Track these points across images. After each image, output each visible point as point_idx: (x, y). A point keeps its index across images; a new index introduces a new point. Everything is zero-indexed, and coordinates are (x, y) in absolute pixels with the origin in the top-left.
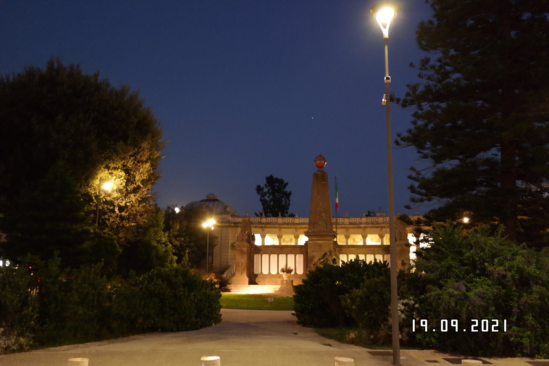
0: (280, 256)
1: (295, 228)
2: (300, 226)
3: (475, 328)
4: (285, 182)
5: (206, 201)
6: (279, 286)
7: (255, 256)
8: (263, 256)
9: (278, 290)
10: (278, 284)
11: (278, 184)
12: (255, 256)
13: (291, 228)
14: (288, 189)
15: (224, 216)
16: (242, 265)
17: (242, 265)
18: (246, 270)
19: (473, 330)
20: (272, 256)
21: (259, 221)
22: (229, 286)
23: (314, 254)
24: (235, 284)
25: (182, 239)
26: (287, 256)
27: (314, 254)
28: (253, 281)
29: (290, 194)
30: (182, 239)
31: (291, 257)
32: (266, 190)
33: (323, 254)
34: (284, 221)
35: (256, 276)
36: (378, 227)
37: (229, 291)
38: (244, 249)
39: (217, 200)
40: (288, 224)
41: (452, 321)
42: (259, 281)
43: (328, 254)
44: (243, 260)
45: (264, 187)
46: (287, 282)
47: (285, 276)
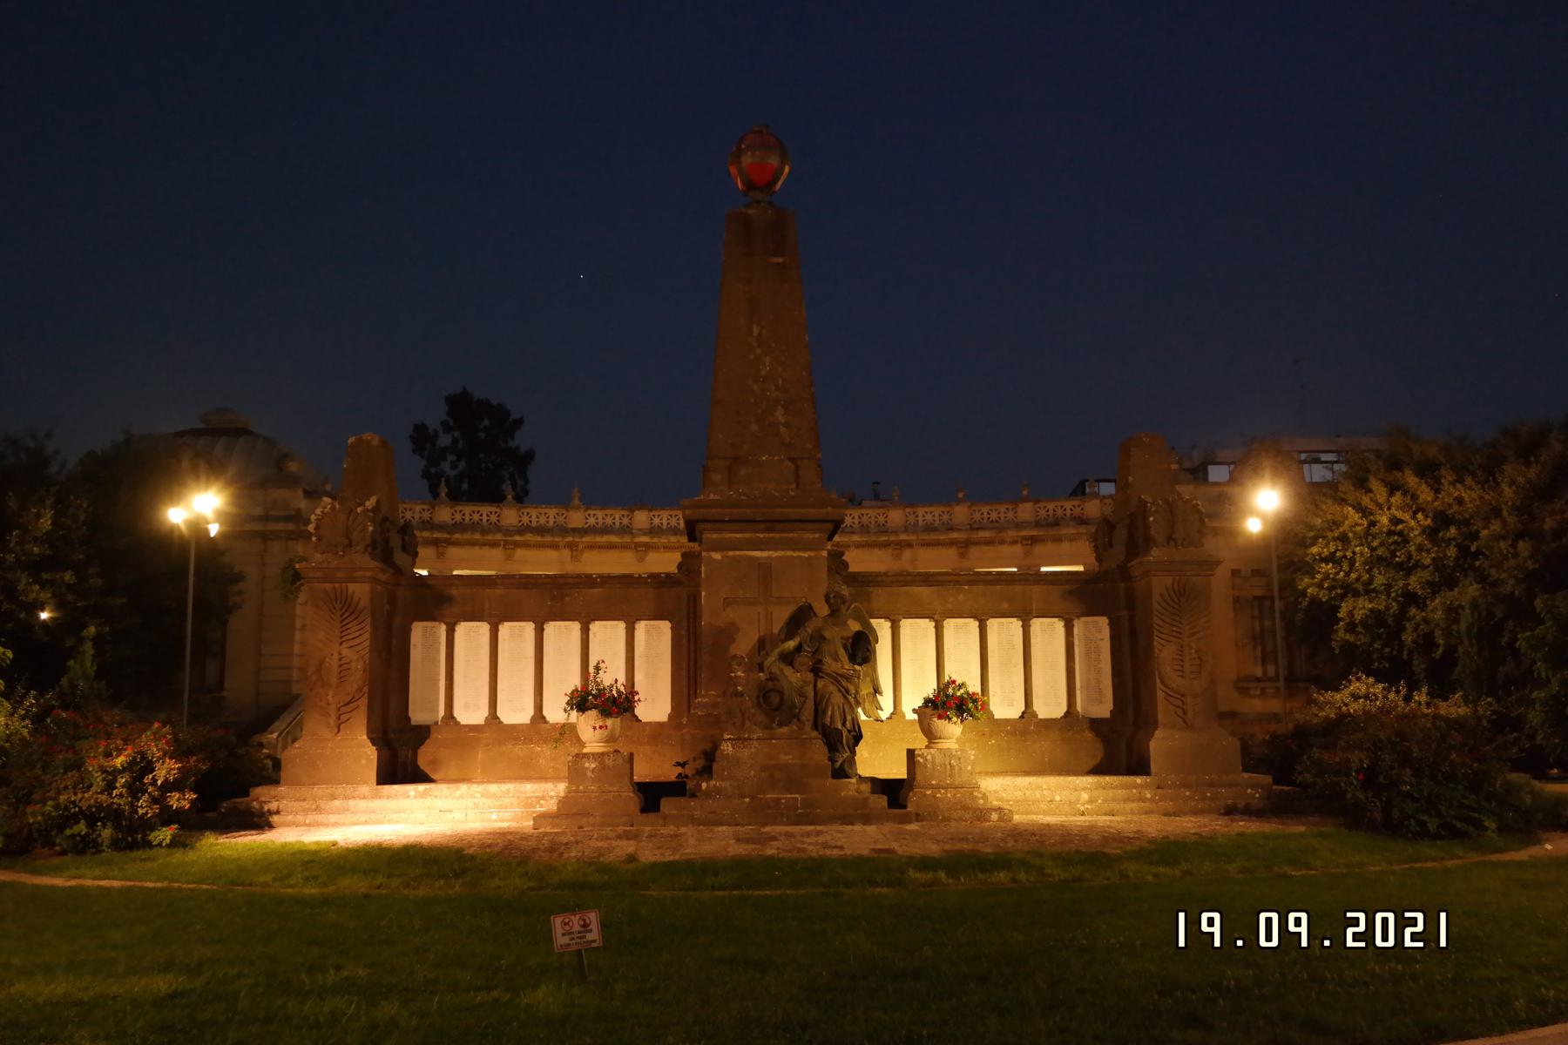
0: (551, 628)
1: (571, 546)
2: (587, 539)
3: (1356, 937)
4: (515, 415)
5: (197, 433)
6: (561, 788)
7: (418, 630)
8: (462, 629)
9: (551, 806)
10: (556, 779)
11: (486, 422)
12: (418, 630)
13: (555, 547)
14: (522, 441)
15: (280, 494)
16: (342, 679)
17: (342, 679)
18: (364, 702)
19: (1350, 943)
20: (505, 629)
21: (426, 515)
22: (263, 796)
23: (731, 614)
24: (297, 783)
25: (68, 577)
26: (585, 632)
27: (731, 614)
28: (403, 760)
29: (529, 456)
30: (68, 577)
31: (608, 637)
32: (444, 440)
33: (781, 615)
34: (525, 520)
35: (423, 733)
36: (885, 545)
37: (260, 822)
38: (352, 587)
39: (246, 432)
40: (541, 530)
41: (1292, 916)
42: (434, 762)
43: (822, 610)
44: (352, 652)
45: (440, 430)
46: (603, 767)
47: (590, 730)
